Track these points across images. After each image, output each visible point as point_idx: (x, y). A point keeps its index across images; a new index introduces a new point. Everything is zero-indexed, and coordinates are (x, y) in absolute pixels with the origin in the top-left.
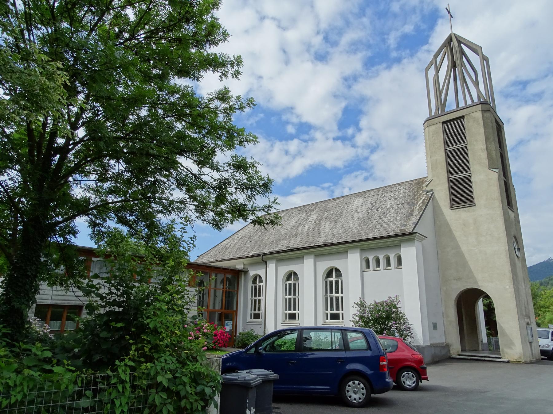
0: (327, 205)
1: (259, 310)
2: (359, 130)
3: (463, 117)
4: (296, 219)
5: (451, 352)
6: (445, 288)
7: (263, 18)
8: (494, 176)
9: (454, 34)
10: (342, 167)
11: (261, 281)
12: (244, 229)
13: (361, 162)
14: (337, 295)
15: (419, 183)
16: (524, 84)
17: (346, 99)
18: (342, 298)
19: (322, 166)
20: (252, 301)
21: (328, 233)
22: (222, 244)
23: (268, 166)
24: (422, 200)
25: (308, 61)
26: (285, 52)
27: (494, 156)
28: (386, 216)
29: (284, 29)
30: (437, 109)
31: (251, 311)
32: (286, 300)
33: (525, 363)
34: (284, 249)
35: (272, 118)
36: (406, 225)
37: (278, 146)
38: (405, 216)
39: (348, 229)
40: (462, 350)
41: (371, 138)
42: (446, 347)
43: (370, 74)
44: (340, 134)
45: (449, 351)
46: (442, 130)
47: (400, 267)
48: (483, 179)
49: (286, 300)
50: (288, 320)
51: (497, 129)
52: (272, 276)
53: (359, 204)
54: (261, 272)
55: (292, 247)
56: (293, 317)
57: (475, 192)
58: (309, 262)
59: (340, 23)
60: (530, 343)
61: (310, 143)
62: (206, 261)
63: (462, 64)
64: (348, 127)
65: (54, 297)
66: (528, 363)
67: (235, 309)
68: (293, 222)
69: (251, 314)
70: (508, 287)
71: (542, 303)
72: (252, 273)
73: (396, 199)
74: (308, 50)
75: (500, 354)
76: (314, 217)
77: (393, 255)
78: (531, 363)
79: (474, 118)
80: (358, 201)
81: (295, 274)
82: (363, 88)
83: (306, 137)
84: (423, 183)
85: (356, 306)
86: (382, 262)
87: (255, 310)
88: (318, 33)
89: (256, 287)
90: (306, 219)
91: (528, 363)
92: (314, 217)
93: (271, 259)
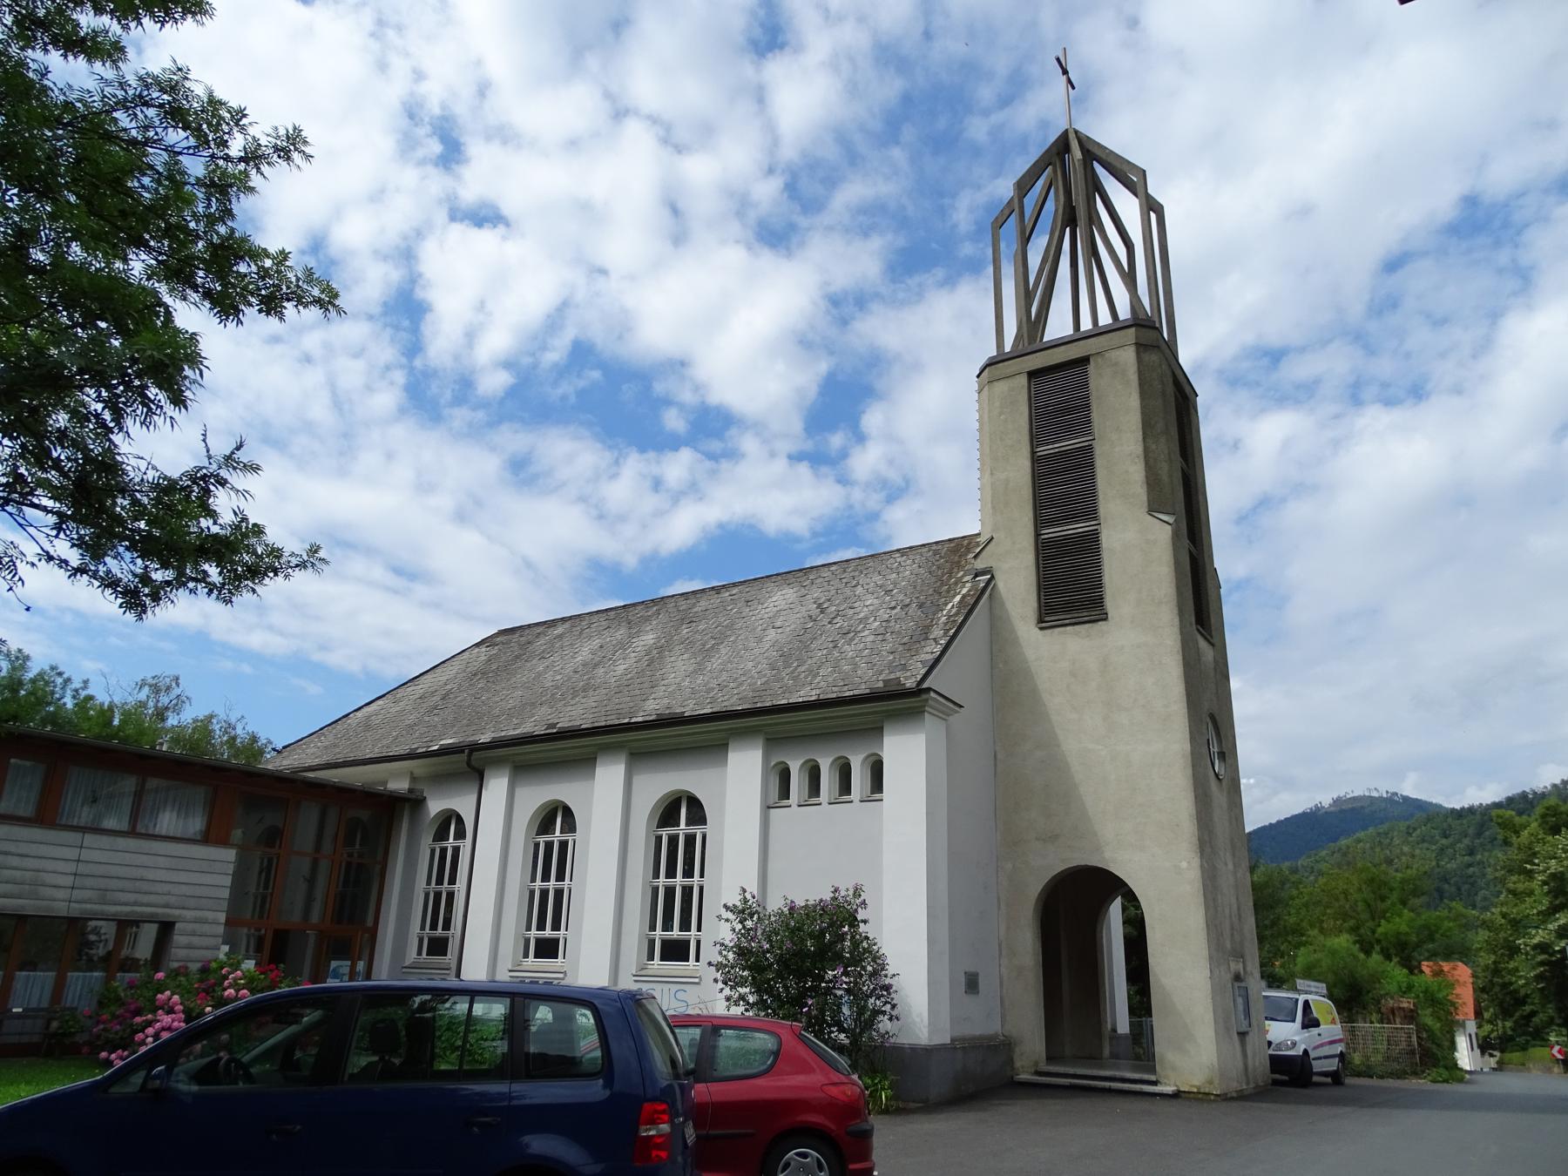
0: (694, 605)
1: (447, 926)
2: (861, 438)
3: (1084, 361)
4: (597, 642)
5: (1018, 1064)
6: (1009, 866)
7: (620, 113)
8: (1160, 533)
9: (1076, 132)
10: (807, 534)
11: (460, 834)
12: (438, 670)
13: (858, 524)
14: (687, 881)
15: (960, 548)
16: (1274, 356)
17: (831, 353)
18: (701, 889)
19: (751, 527)
20: (427, 895)
21: (682, 687)
22: (359, 714)
23: (601, 517)
24: (958, 598)
25: (737, 242)
26: (675, 211)
27: (1165, 478)
28: (852, 639)
29: (680, 149)
30: (1018, 337)
31: (423, 928)
32: (532, 893)
33: (1225, 1098)
34: (540, 730)
35: (625, 387)
36: (904, 667)
37: (634, 465)
38: (906, 640)
39: (740, 670)
40: (1051, 1058)
41: (891, 462)
42: (1002, 1047)
43: (901, 295)
44: (809, 446)
45: (1011, 1061)
46: (1026, 397)
47: (877, 796)
48: (1133, 544)
49: (532, 893)
50: (531, 962)
51: (1174, 409)
52: (497, 814)
53: (782, 604)
54: (463, 804)
55: (564, 723)
56: (548, 949)
57: (1106, 579)
58: (610, 776)
59: (831, 153)
60: (1242, 1035)
61: (725, 465)
62: (296, 764)
63: (1093, 219)
64: (832, 427)
65: (77, 894)
66: (1232, 1099)
67: (370, 923)
68: (585, 652)
69: (421, 941)
70: (1184, 864)
71: (1292, 920)
72: (435, 806)
73: (888, 592)
74: (740, 214)
75: (1153, 1070)
76: (649, 638)
77: (862, 756)
78: (1241, 1097)
79: (1116, 364)
80: (781, 597)
81: (568, 812)
82: (882, 330)
83: (715, 446)
84: (968, 550)
85: (730, 915)
86: (827, 780)
87: (434, 927)
88: (771, 171)
89: (444, 851)
90: (622, 646)
91: (1232, 1099)
92: (649, 638)
93: (498, 763)
